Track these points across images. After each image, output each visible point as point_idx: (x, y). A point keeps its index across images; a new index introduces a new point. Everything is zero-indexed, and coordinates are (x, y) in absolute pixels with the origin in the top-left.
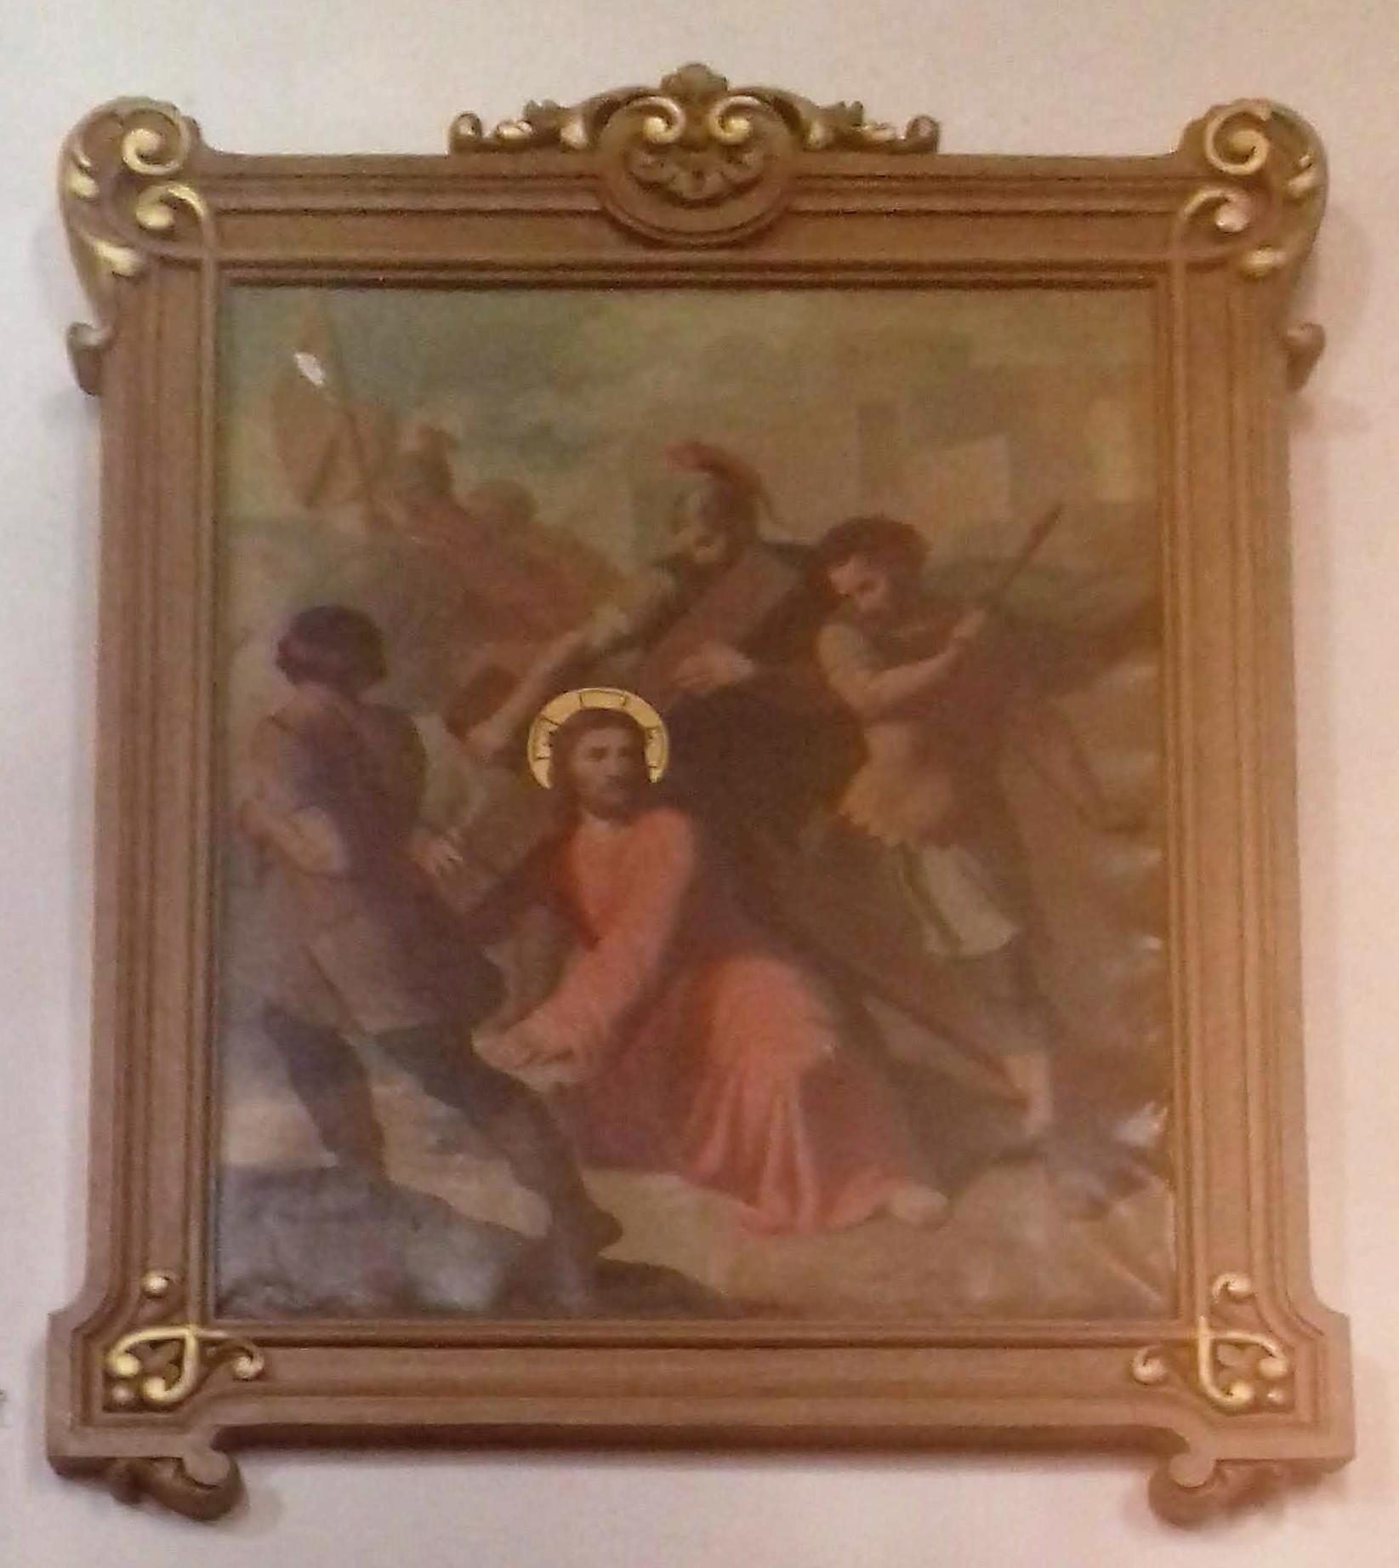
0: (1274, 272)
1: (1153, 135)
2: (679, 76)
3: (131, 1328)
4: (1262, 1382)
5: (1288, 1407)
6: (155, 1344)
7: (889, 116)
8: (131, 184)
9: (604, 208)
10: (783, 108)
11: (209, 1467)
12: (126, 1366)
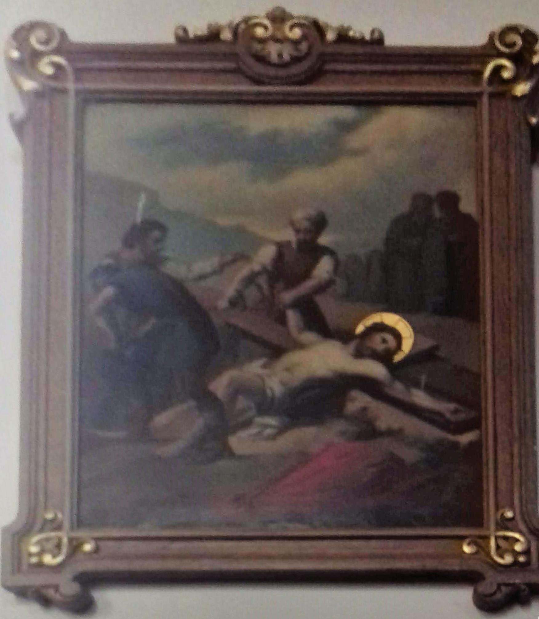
0: (472, 444)
2: (272, 13)
4: (516, 554)
6: (47, 540)
7: (361, 28)
8: (36, 55)
10: (317, 28)
12: (34, 549)
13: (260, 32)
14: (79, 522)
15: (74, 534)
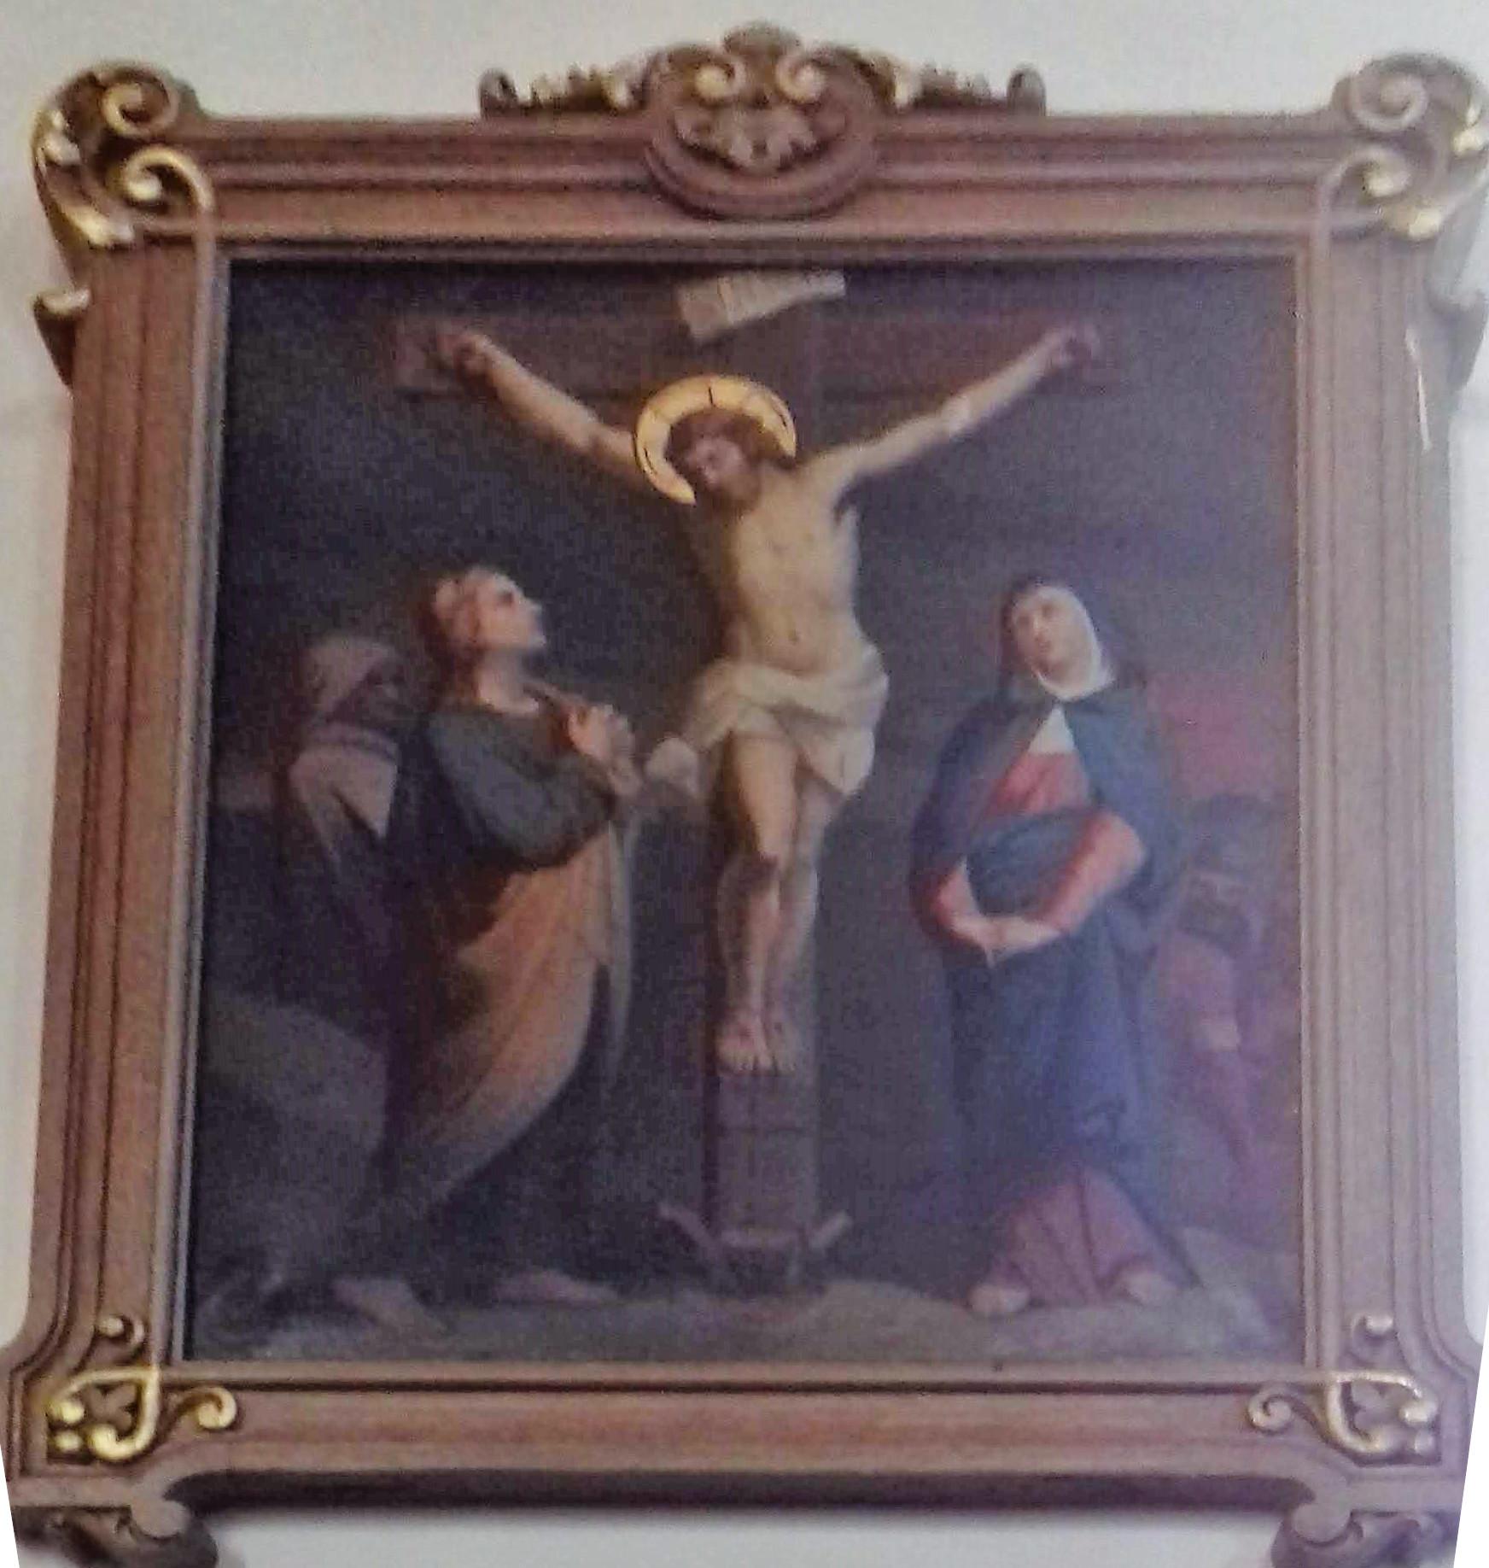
1: (1296, 87)
6: (106, 1389)
9: (652, 177)
10: (872, 76)
12: (72, 1413)
13: (710, 81)
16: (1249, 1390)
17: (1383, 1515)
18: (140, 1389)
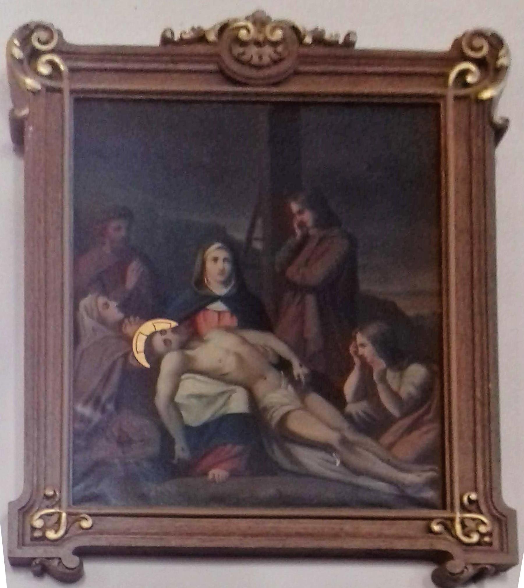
1: (442, 44)
3: (38, 510)
5: (490, 544)
7: (335, 30)
10: (295, 29)
11: (72, 562)
12: (38, 523)
13: (243, 33)
14: (78, 501)
15: (74, 510)
16: (431, 519)
17: (474, 565)
18: (60, 514)
